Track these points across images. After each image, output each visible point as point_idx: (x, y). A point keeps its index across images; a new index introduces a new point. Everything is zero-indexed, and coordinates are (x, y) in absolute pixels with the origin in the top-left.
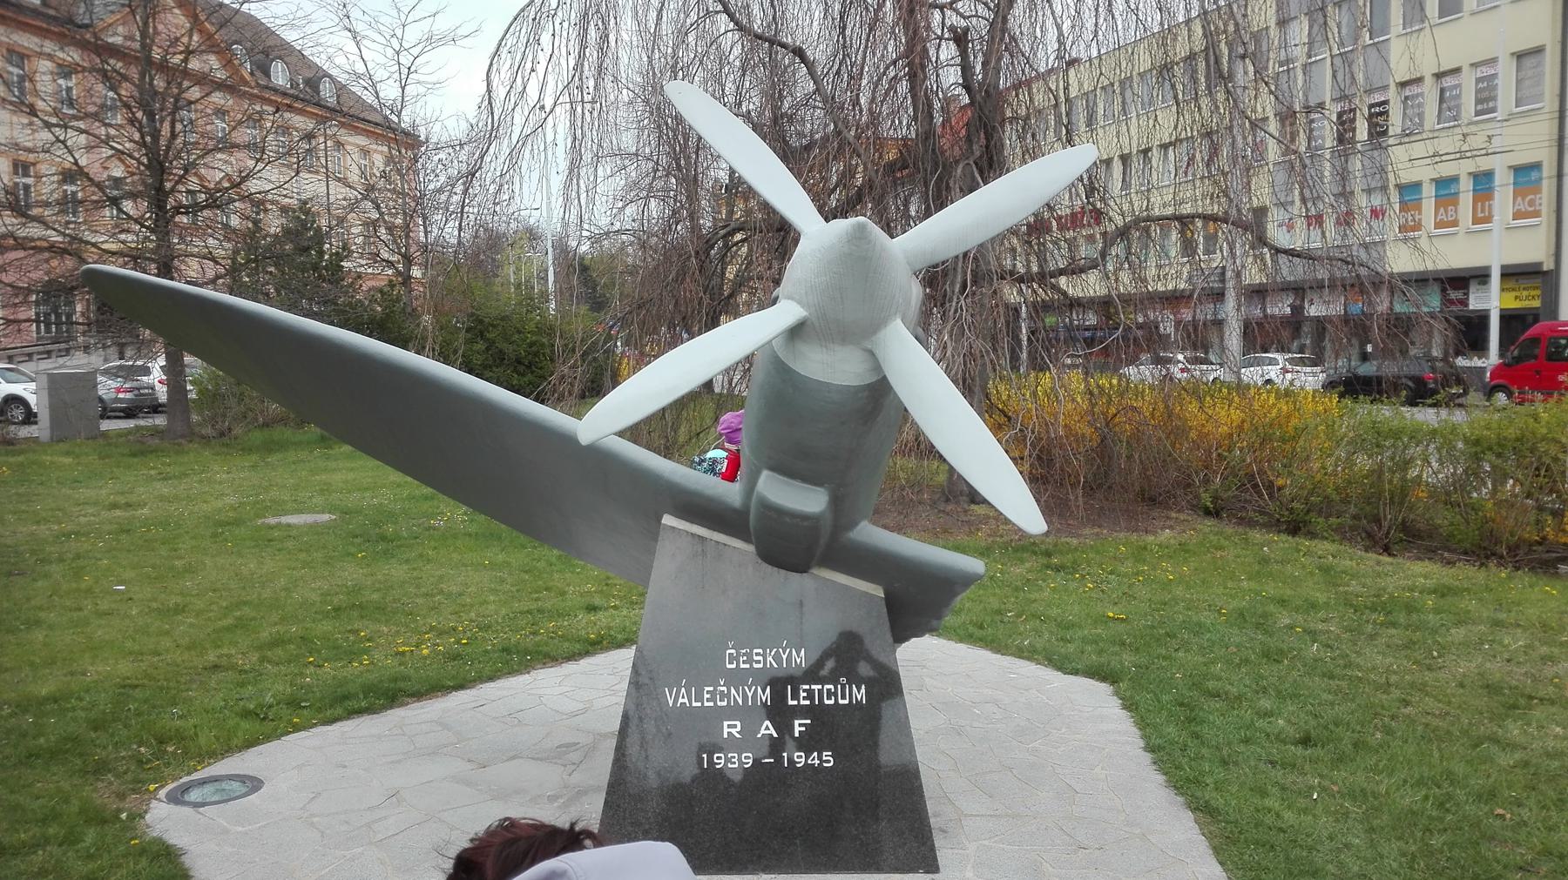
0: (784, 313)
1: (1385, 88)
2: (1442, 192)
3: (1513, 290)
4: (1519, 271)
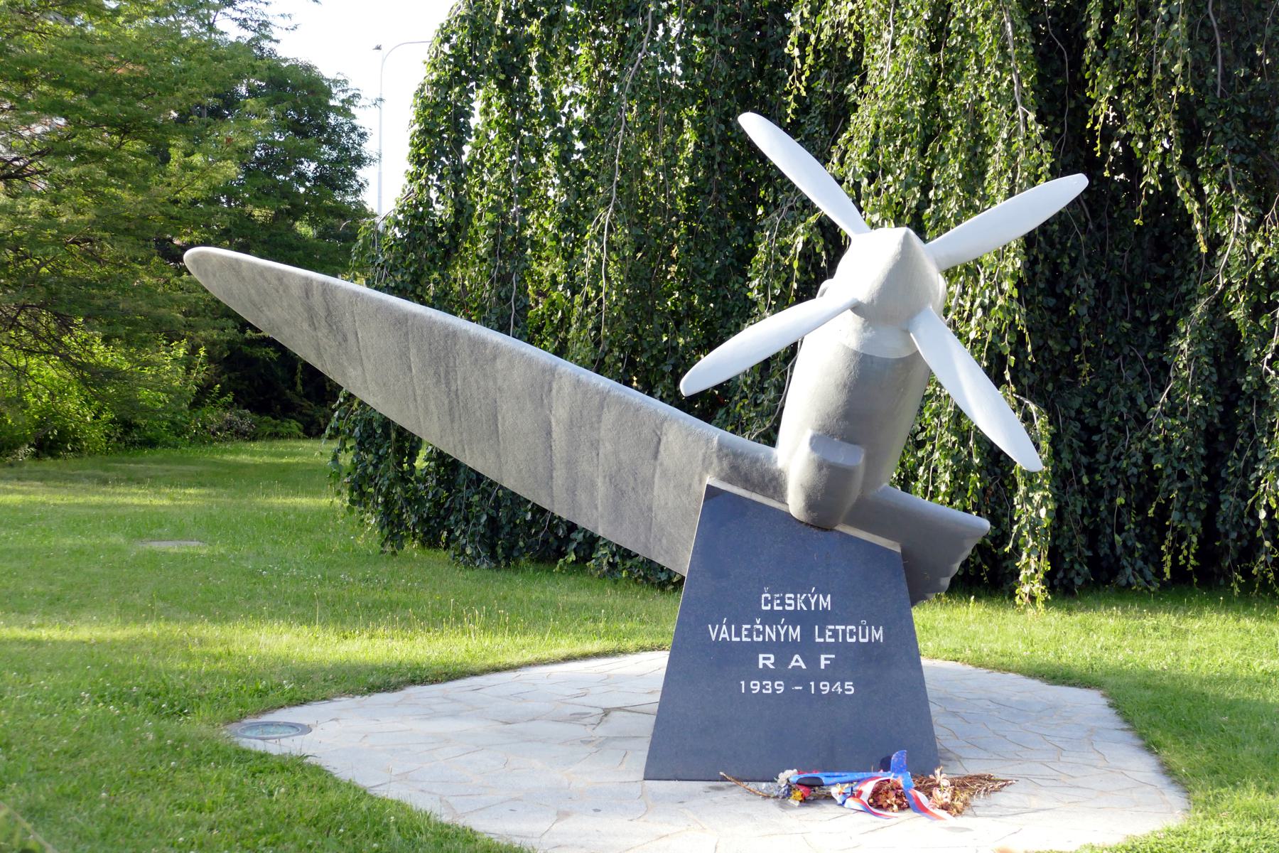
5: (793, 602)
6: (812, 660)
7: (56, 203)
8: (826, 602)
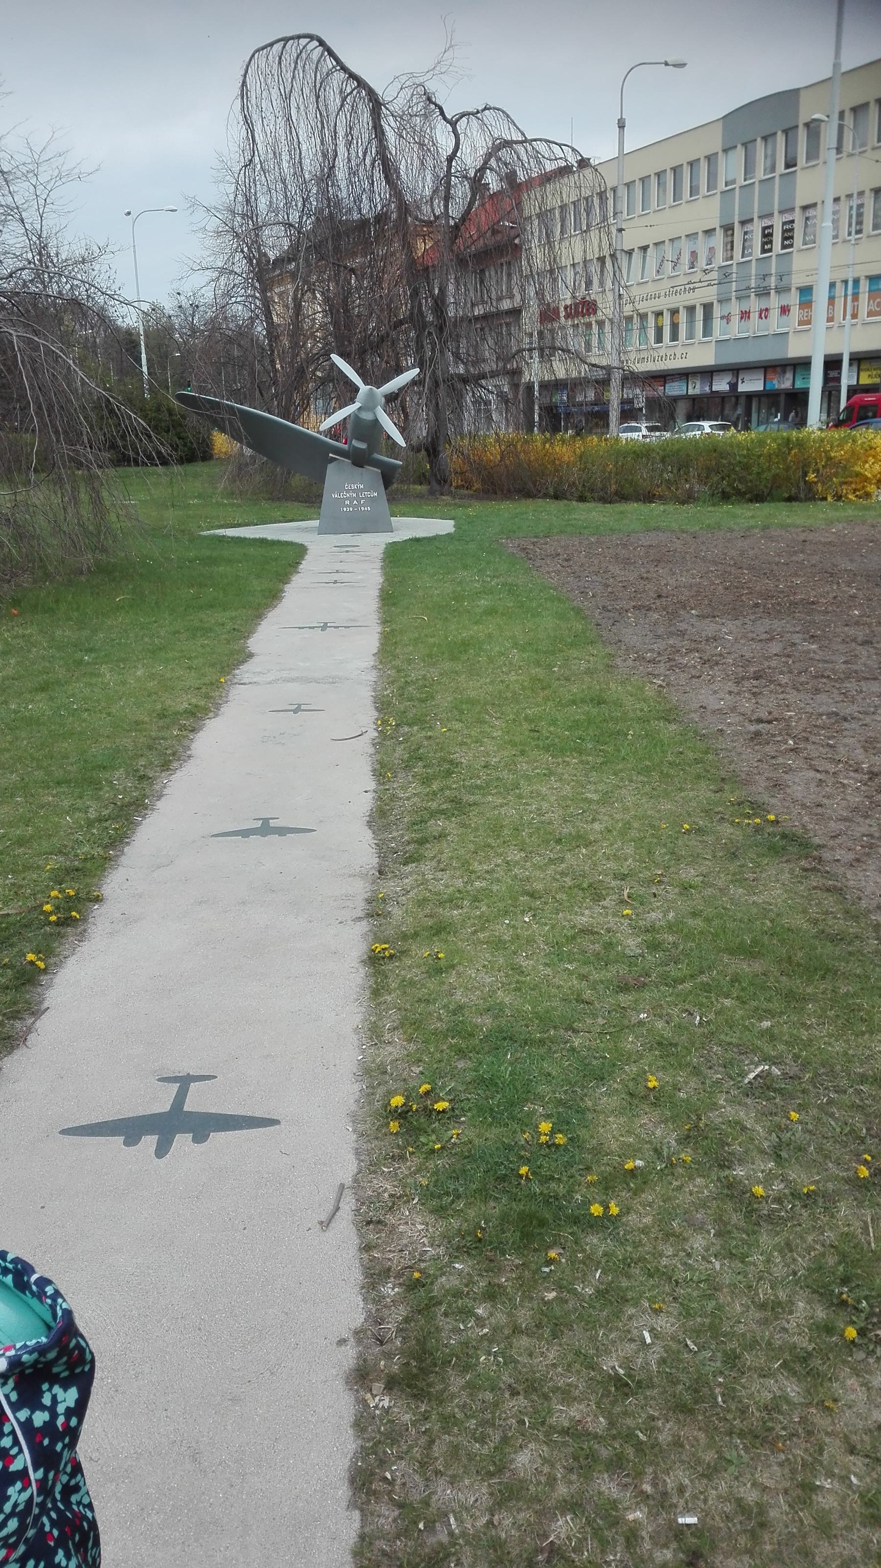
0: (357, 405)
1: (792, 209)
2: (874, 287)
3: (868, 370)
4: (867, 356)
5: (354, 487)
6: (359, 502)
7: (721, 730)
8: (362, 487)
